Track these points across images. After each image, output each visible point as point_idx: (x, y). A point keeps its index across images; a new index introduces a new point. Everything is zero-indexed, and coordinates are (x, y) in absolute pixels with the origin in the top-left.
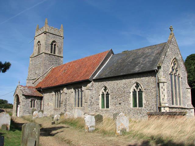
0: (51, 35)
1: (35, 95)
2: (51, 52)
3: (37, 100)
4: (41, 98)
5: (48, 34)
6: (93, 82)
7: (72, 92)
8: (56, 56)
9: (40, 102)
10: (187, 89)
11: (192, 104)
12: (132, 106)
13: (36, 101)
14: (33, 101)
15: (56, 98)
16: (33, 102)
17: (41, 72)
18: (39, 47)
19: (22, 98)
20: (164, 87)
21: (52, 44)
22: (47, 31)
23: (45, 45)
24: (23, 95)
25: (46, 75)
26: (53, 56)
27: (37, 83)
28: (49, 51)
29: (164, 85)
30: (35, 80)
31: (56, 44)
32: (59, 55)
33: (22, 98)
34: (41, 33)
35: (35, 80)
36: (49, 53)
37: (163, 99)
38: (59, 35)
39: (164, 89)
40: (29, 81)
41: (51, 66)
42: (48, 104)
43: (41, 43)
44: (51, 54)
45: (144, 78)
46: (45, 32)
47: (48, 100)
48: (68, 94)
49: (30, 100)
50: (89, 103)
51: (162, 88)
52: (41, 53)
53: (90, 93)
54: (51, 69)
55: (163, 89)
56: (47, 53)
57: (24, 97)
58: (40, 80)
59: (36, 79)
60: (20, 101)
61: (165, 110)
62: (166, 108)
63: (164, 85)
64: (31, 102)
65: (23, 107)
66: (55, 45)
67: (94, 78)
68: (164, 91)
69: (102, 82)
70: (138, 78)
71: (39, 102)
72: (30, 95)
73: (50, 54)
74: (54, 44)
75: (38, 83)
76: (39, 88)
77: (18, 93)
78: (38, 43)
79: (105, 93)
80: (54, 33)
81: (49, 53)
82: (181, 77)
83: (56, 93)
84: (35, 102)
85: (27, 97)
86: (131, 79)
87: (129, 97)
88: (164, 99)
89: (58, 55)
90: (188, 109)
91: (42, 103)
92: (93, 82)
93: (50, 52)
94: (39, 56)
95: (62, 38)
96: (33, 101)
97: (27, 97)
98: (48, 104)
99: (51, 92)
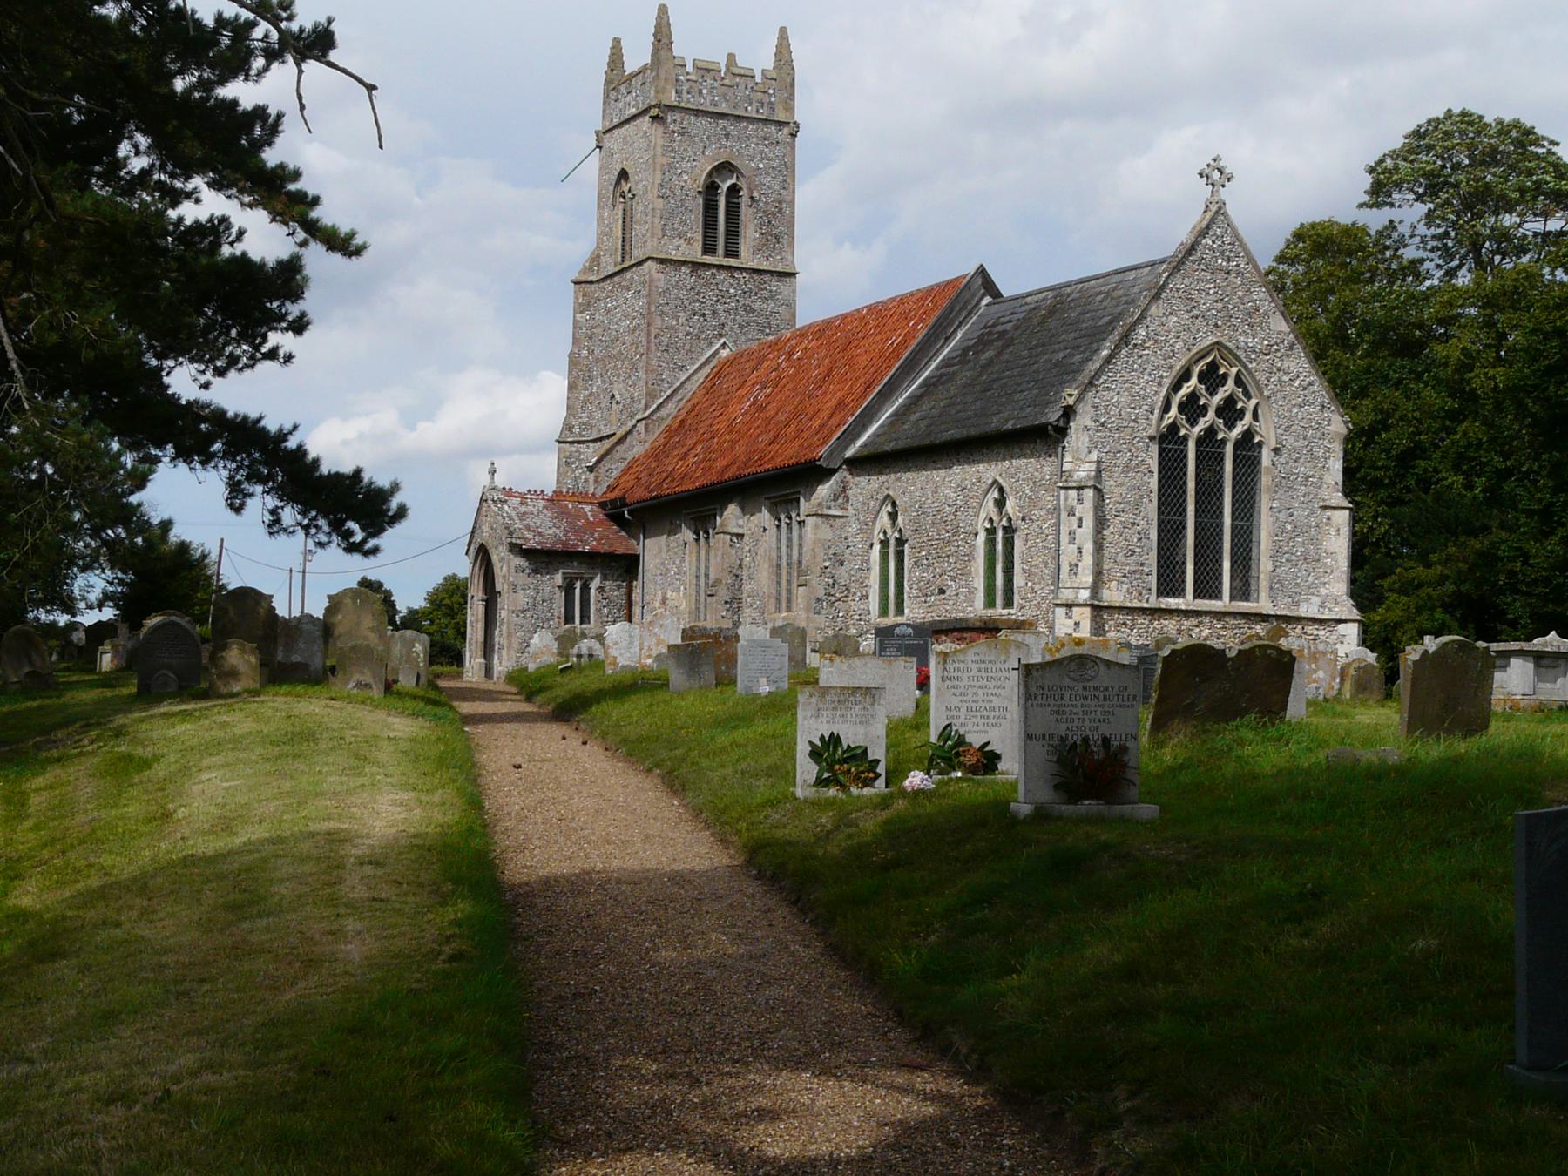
0: (704, 122)
1: (587, 549)
2: (709, 249)
3: (605, 578)
4: (627, 567)
5: (677, 116)
6: (846, 474)
7: (765, 529)
8: (741, 269)
9: (624, 590)
10: (1329, 513)
11: (1353, 594)
12: (874, 603)
13: (595, 585)
14: (578, 585)
15: (698, 560)
16: (578, 591)
17: (640, 392)
18: (628, 208)
19: (506, 566)
20: (1079, 510)
21: (711, 189)
22: (672, 99)
23: (660, 203)
24: (516, 549)
25: (671, 408)
26: (722, 275)
27: (614, 469)
28: (689, 241)
29: (1080, 501)
30: (607, 444)
31: (743, 184)
32: (765, 266)
33: (506, 566)
34: (633, 111)
35: (607, 444)
36: (695, 252)
37: (1074, 567)
38: (764, 113)
39: (1080, 519)
40: (573, 448)
41: (711, 344)
42: (664, 601)
43: (636, 184)
44: (709, 259)
45: (1022, 462)
46: (654, 112)
47: (665, 574)
48: (746, 538)
49: (559, 579)
50: (818, 586)
51: (1071, 513)
52: (638, 254)
53: (826, 533)
54: (707, 370)
55: (1074, 520)
56: (674, 255)
57: (523, 562)
58: (636, 448)
59: (615, 439)
60: (498, 587)
61: (1071, 618)
62: (1075, 609)
63: (1080, 501)
64: (568, 589)
65: (519, 620)
66: (734, 190)
67: (849, 453)
68: (1080, 526)
69: (883, 478)
70: (1004, 459)
71: (619, 587)
72: (559, 547)
73: (696, 266)
74: (725, 186)
75: (623, 465)
76: (613, 501)
77: (485, 535)
78: (618, 183)
79: (893, 535)
80: (723, 108)
81: (695, 252)
82: (1273, 444)
83: (698, 535)
84: (593, 591)
85: (541, 559)
86: (981, 467)
87: (971, 555)
88: (1077, 566)
89: (754, 265)
90: (1321, 622)
91: (636, 596)
92: (843, 474)
93: (699, 246)
94: (628, 275)
95: (786, 130)
96: (578, 585)
97: (541, 559)
98: (664, 601)
99: (673, 531)
